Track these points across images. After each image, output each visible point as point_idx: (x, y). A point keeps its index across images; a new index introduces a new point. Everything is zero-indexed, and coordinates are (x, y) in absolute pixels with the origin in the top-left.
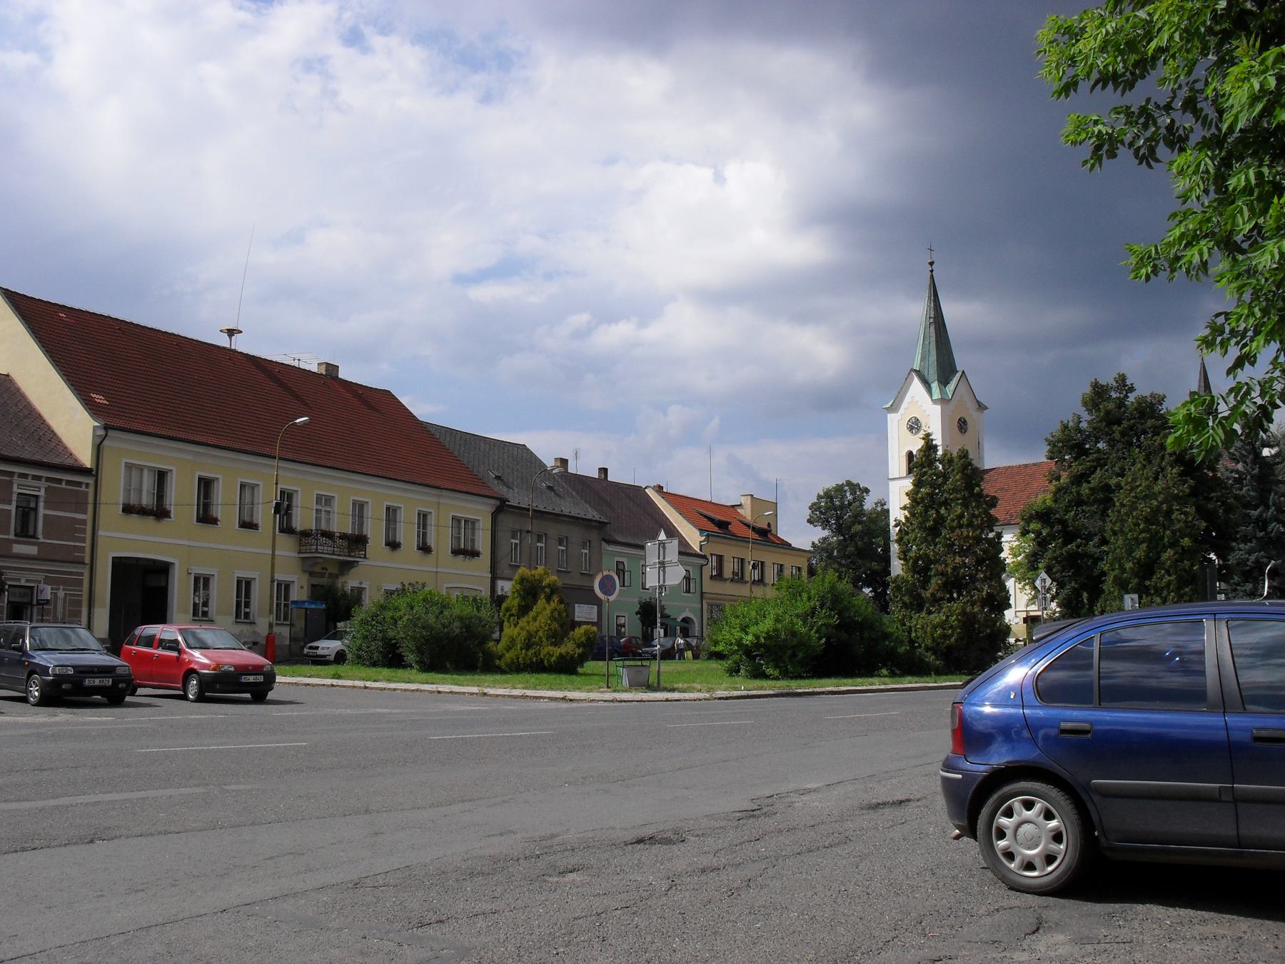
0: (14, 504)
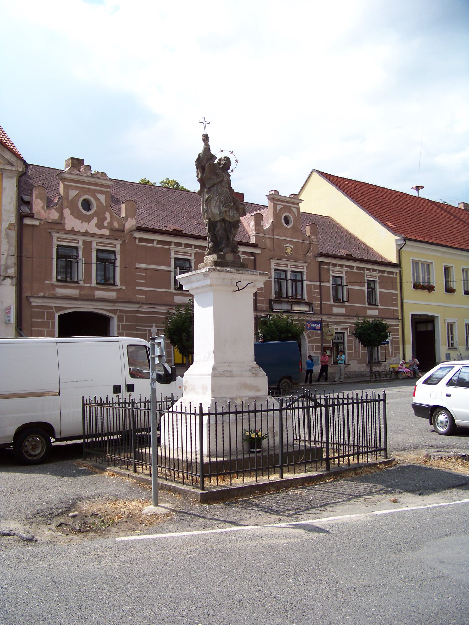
0: (331, 283)
